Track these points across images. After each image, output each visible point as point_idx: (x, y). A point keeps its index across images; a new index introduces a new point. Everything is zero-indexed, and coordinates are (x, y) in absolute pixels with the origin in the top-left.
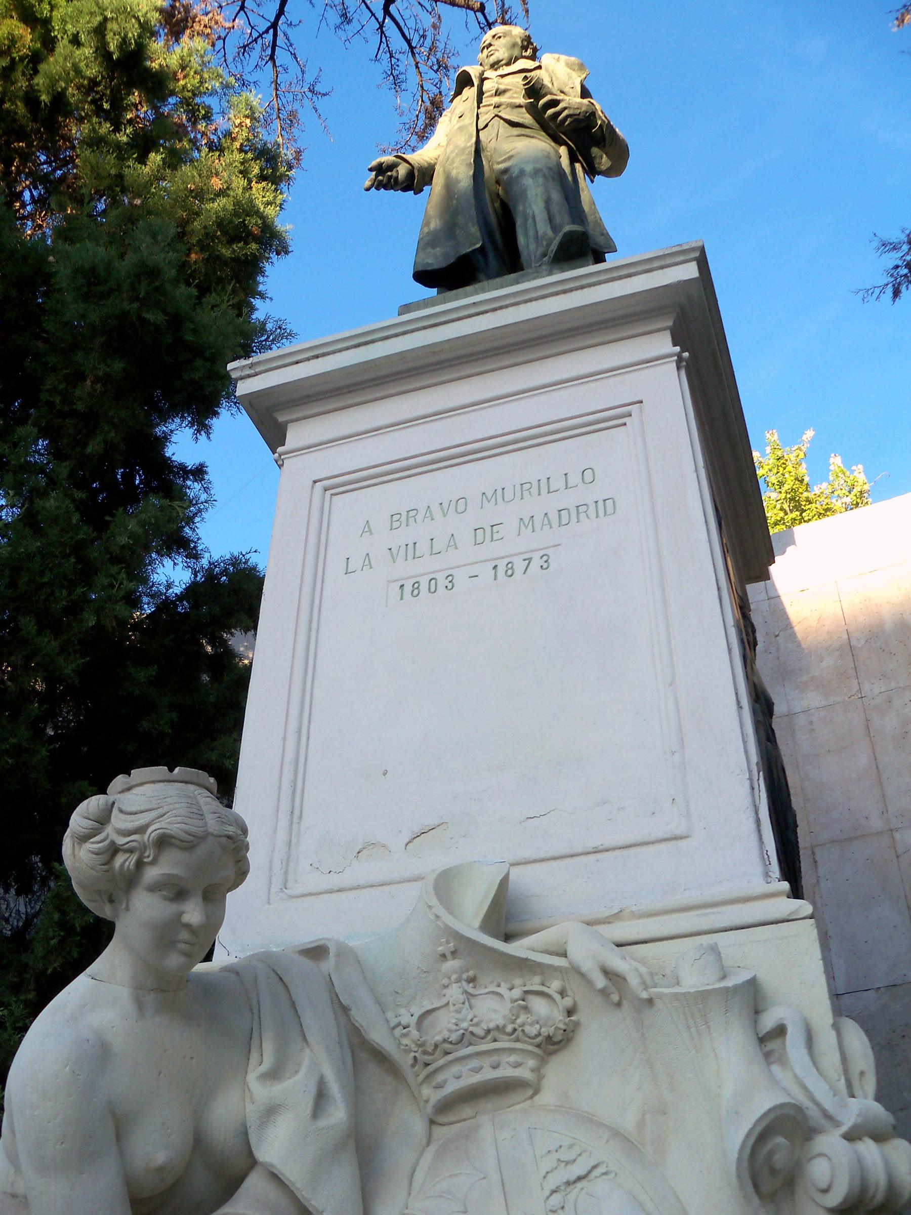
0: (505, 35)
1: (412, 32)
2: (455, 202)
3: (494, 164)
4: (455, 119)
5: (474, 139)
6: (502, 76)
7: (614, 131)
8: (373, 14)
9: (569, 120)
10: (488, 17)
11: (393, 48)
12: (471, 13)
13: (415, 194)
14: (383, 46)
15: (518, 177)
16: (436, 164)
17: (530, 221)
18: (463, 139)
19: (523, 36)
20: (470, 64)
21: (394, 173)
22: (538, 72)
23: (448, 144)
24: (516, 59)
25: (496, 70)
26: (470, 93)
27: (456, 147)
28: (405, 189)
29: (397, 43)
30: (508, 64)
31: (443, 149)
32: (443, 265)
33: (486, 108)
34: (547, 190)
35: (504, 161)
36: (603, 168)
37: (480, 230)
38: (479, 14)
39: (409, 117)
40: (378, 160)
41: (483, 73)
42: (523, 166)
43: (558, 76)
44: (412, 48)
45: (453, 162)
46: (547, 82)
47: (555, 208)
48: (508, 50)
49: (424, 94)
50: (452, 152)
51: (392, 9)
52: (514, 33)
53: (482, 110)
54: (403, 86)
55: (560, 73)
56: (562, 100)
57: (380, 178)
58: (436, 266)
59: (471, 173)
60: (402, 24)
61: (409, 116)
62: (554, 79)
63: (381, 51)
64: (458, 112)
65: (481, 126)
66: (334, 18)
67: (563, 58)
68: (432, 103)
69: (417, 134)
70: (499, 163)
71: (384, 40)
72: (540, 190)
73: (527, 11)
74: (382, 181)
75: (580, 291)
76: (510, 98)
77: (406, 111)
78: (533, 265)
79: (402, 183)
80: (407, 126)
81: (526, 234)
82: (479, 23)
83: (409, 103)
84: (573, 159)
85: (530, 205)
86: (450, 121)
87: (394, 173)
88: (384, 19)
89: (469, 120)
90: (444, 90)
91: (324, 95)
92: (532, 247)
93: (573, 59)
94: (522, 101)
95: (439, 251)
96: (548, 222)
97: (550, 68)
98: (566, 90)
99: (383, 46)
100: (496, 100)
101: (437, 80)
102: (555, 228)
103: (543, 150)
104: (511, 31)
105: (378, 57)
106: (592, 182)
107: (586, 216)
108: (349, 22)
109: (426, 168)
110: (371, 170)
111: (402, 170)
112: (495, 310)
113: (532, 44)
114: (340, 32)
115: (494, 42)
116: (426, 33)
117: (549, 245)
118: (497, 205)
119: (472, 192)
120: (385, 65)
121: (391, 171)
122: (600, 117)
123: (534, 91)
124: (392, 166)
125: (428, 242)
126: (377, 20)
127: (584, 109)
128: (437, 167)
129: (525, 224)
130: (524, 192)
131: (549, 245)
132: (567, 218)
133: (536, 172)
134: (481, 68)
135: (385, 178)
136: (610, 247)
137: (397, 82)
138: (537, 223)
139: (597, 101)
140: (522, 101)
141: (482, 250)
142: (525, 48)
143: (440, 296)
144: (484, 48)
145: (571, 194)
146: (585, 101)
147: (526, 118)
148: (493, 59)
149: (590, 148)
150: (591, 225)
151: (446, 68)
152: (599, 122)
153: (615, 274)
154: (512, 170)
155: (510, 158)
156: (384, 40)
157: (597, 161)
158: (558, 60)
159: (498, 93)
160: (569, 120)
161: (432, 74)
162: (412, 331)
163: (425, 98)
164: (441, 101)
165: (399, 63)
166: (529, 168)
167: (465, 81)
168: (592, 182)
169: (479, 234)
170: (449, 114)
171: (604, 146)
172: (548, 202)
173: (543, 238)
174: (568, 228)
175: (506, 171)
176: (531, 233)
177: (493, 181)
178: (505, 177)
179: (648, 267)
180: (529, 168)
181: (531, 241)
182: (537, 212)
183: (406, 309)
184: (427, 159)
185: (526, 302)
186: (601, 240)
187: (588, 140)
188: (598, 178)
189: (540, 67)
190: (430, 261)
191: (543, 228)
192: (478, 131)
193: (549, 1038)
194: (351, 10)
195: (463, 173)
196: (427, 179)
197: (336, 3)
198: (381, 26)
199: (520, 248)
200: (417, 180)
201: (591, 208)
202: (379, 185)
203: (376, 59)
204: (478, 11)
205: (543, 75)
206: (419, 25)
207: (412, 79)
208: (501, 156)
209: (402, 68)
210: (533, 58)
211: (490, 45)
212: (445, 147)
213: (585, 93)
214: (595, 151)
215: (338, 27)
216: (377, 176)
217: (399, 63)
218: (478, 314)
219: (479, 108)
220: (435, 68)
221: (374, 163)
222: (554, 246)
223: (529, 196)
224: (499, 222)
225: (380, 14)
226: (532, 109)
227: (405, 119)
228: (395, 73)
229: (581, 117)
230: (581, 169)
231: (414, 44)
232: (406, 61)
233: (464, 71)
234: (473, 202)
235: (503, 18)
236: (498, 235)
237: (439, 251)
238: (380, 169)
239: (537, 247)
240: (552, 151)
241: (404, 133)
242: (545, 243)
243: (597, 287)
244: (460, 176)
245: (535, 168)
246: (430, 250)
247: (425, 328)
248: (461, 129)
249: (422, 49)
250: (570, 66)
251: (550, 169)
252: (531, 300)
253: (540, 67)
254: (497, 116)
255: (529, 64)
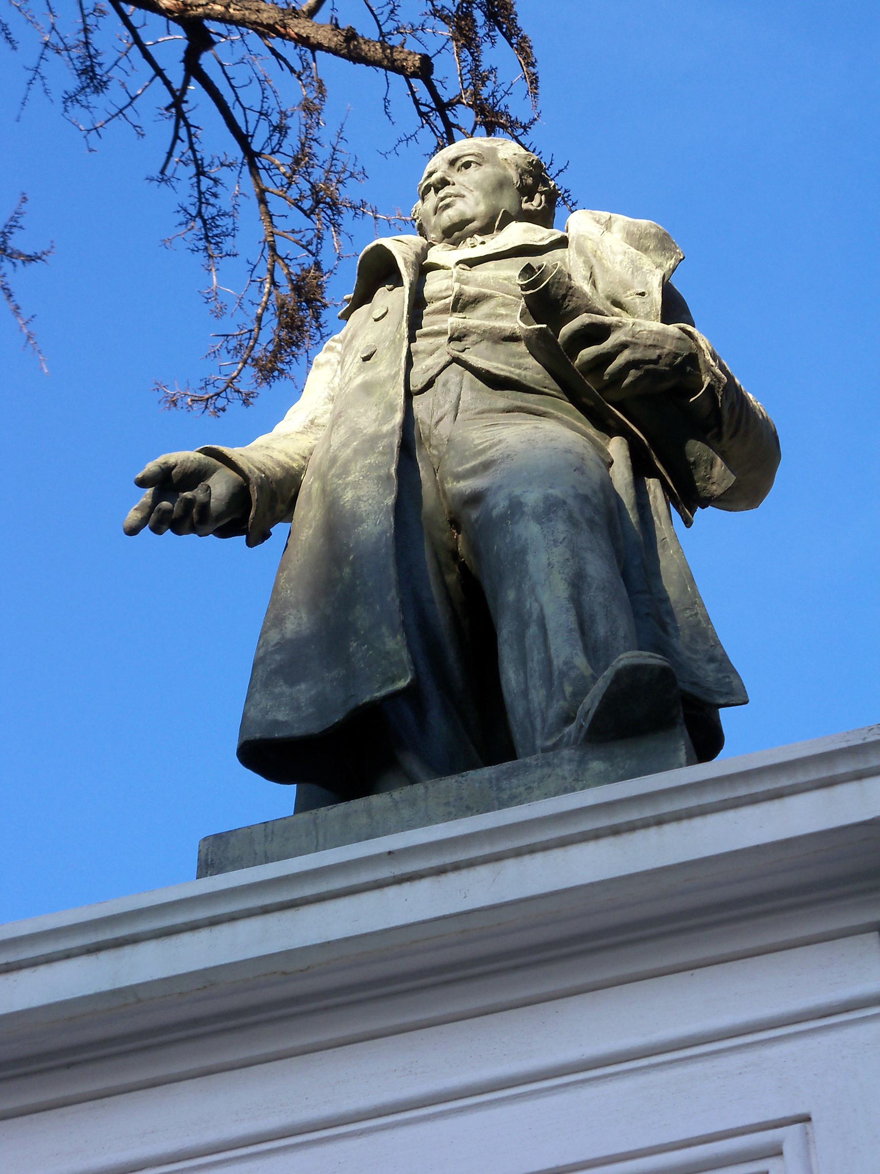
0: (480, 160)
1: (253, 117)
2: (347, 570)
3: (447, 480)
4: (354, 360)
5: (398, 417)
6: (472, 263)
7: (743, 400)
8: (159, 72)
9: (633, 374)
10: (440, 90)
11: (205, 152)
12: (397, 79)
13: (250, 543)
14: (182, 147)
15: (503, 517)
16: (303, 469)
17: (533, 630)
18: (372, 414)
19: (523, 164)
20: (392, 229)
21: (198, 494)
22: (558, 253)
23: (335, 423)
24: (507, 219)
25: (456, 243)
26: (392, 300)
27: (354, 432)
28: (224, 532)
29: (215, 141)
30: (487, 229)
31: (321, 434)
32: (314, 727)
33: (431, 340)
34: (575, 553)
35: (473, 472)
36: (716, 490)
37: (409, 646)
38: (418, 84)
39: (237, 321)
40: (161, 459)
41: (423, 254)
42: (518, 491)
43: (608, 264)
44: (251, 156)
45: (345, 471)
46: (580, 282)
47: (595, 598)
48: (486, 195)
49: (279, 265)
50: (344, 445)
51: (207, 61)
52: (501, 155)
53: (421, 344)
54: (228, 244)
55: (608, 254)
56: (618, 326)
57: (165, 504)
58: (298, 730)
59: (390, 500)
60: (228, 97)
61: (240, 318)
62: (597, 271)
63: (175, 159)
64: (361, 346)
65: (417, 381)
66: (63, 76)
67: (621, 220)
68: (297, 289)
69: (256, 362)
70: (458, 477)
71: (183, 133)
72: (559, 553)
73: (534, 81)
74: (170, 512)
75: (653, 832)
76: (489, 316)
77: (233, 307)
78: (538, 742)
79: (220, 516)
80: (234, 343)
81: (523, 661)
82: (417, 102)
83: (240, 288)
84: (641, 468)
85: (533, 590)
86: (342, 363)
87: (198, 494)
88: (186, 82)
89: (388, 368)
90: (327, 260)
91: (31, 259)
92: (538, 696)
93: (644, 222)
94: (515, 323)
95: (304, 691)
96: (577, 635)
97: (589, 245)
98: (627, 298)
99: (182, 147)
100: (453, 321)
101: (310, 235)
102: (595, 651)
103: (568, 451)
104: (493, 151)
105: (168, 172)
106: (688, 523)
107: (670, 613)
108: (100, 86)
109: (279, 482)
110: (142, 483)
111: (220, 486)
112: (441, 871)
113: (545, 183)
114: (76, 111)
115: (456, 177)
116: (289, 122)
117: (579, 694)
118: (452, 578)
119: (392, 551)
120: (184, 191)
121: (191, 488)
122: (709, 369)
123: (548, 300)
124: (196, 476)
125: (277, 666)
126: (167, 83)
127: (669, 347)
128: (307, 480)
129: (520, 637)
130: (521, 554)
131: (579, 694)
132: (624, 625)
133: (550, 508)
134: (417, 241)
135: (176, 502)
136: (731, 693)
137: (211, 233)
138: (546, 591)
139: (701, 331)
140: (515, 323)
141: (412, 693)
142: (527, 192)
143: (305, 816)
144: (427, 189)
145: (634, 557)
146: (673, 329)
147: (527, 367)
148: (449, 216)
149: (686, 442)
150: (685, 634)
151: (334, 206)
152: (707, 380)
153: (743, 791)
154: (491, 500)
155: (486, 466)
156: (183, 133)
157: (701, 472)
158: (608, 225)
159: (462, 304)
160: (633, 374)
161: (298, 220)
162: (233, 918)
163: (281, 275)
164: (320, 286)
165: (219, 190)
166: (532, 497)
167: (379, 271)
168: (688, 523)
169: (405, 655)
170: (339, 347)
171: (719, 436)
172: (578, 583)
173: (563, 675)
174: (626, 658)
175: (475, 499)
176: (536, 658)
177: (442, 520)
178: (474, 514)
179: (824, 773)
180: (532, 497)
181: (535, 681)
182: (549, 610)
183: (217, 854)
184: (282, 458)
185: (518, 853)
186: (708, 673)
187: (681, 422)
188: (703, 515)
189: (562, 243)
190: (281, 717)
191: (565, 650)
192: (409, 395)
193: (608, 650)
194: (106, 59)
195: (368, 497)
196: (281, 507)
197: (71, 41)
198: (178, 100)
199: (508, 698)
200: (257, 507)
201: (684, 590)
202: (159, 521)
203: (163, 177)
204: (414, 75)
205: (570, 263)
206: (272, 103)
207: (249, 231)
208: (464, 459)
209: (224, 202)
210: (544, 218)
211: (444, 183)
212: (323, 420)
213: (673, 307)
214: (696, 448)
215: (71, 99)
216: (157, 498)
217: (219, 190)
218: (399, 880)
219: (412, 338)
220: (307, 204)
221: (151, 466)
222: (591, 702)
223: (532, 568)
224: (455, 620)
225: (176, 73)
226: (542, 346)
227: (229, 325)
228: (208, 212)
229: (662, 367)
230: (659, 492)
231: (256, 147)
232: (235, 187)
233: (380, 247)
234: (392, 572)
235: (476, 94)
236: (451, 655)
237: (304, 691)
238: (165, 482)
239: (550, 697)
240: (590, 453)
241: (226, 360)
242: (568, 689)
243: (698, 822)
244: (364, 507)
245: (546, 498)
246: (282, 688)
247: (266, 910)
248: (367, 388)
249: (277, 160)
250: (637, 241)
251: (585, 499)
252: (532, 850)
253: (562, 243)
254: (456, 360)
255: (537, 235)
